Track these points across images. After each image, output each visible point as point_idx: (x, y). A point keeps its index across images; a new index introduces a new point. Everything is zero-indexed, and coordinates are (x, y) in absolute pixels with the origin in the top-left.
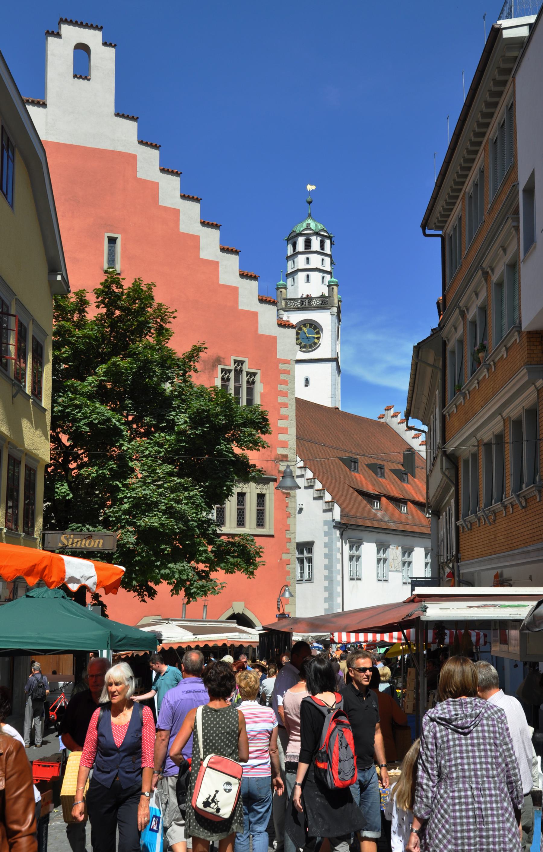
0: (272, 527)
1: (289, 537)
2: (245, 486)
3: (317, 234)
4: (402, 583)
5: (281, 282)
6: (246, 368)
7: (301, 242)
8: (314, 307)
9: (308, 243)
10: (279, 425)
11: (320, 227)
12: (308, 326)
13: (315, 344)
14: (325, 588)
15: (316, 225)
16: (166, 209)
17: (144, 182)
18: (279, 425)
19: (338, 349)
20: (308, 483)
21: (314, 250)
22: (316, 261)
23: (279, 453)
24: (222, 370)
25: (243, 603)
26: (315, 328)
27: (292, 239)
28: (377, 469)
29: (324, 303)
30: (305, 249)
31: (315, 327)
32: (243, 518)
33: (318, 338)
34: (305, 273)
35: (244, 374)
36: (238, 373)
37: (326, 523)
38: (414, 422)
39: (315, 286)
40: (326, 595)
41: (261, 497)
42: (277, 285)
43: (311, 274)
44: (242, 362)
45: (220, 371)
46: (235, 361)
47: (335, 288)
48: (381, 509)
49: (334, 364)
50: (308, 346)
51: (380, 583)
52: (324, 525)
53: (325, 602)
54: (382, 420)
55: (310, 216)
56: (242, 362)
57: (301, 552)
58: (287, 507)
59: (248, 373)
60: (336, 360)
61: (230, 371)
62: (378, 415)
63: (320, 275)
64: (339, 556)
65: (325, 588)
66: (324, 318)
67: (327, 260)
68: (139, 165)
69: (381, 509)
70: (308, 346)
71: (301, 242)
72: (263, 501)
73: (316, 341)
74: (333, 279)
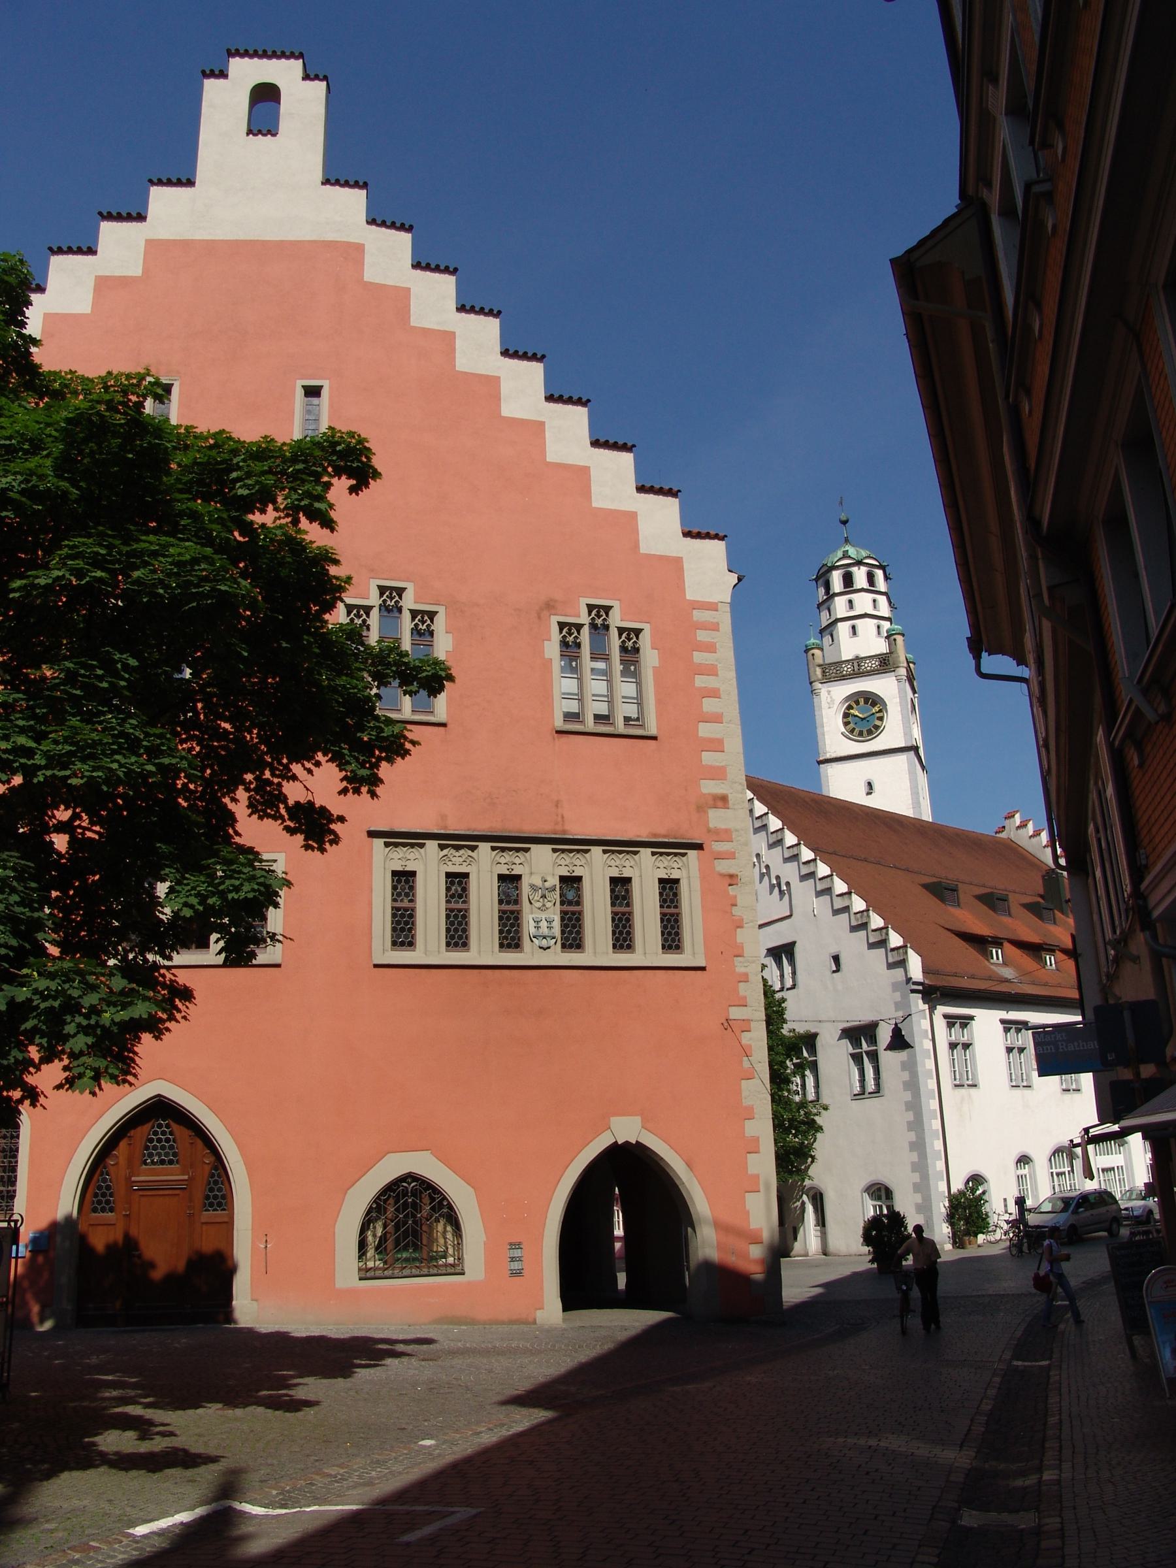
0: (700, 948)
1: (743, 970)
2: (627, 864)
3: (859, 563)
4: (1059, 1090)
5: (812, 641)
6: (616, 619)
7: (836, 579)
9: (848, 580)
10: (701, 734)
11: (864, 553)
12: (862, 701)
13: (877, 727)
14: (907, 1103)
16: (426, 332)
17: (378, 290)
18: (701, 734)
19: (916, 733)
20: (857, 920)
21: (859, 587)
22: (863, 603)
23: (705, 790)
24: (562, 626)
25: (638, 1119)
27: (823, 577)
28: (993, 901)
29: (885, 664)
31: (872, 699)
33: (881, 719)
35: (614, 633)
36: (599, 630)
37: (895, 987)
38: (995, 663)
39: (866, 642)
40: (910, 1116)
41: (669, 888)
44: (607, 609)
47: (899, 639)
48: (1005, 964)
50: (865, 733)
51: (1017, 1092)
52: (894, 991)
53: (909, 1130)
54: (1003, 835)
55: (847, 541)
57: (856, 1043)
59: (621, 630)
60: (915, 749)
62: (996, 829)
64: (928, 1045)
65: (907, 1103)
66: (887, 687)
67: (882, 600)
68: (368, 259)
69: (1005, 964)
70: (865, 733)
71: (836, 579)
72: (675, 895)
73: (878, 723)
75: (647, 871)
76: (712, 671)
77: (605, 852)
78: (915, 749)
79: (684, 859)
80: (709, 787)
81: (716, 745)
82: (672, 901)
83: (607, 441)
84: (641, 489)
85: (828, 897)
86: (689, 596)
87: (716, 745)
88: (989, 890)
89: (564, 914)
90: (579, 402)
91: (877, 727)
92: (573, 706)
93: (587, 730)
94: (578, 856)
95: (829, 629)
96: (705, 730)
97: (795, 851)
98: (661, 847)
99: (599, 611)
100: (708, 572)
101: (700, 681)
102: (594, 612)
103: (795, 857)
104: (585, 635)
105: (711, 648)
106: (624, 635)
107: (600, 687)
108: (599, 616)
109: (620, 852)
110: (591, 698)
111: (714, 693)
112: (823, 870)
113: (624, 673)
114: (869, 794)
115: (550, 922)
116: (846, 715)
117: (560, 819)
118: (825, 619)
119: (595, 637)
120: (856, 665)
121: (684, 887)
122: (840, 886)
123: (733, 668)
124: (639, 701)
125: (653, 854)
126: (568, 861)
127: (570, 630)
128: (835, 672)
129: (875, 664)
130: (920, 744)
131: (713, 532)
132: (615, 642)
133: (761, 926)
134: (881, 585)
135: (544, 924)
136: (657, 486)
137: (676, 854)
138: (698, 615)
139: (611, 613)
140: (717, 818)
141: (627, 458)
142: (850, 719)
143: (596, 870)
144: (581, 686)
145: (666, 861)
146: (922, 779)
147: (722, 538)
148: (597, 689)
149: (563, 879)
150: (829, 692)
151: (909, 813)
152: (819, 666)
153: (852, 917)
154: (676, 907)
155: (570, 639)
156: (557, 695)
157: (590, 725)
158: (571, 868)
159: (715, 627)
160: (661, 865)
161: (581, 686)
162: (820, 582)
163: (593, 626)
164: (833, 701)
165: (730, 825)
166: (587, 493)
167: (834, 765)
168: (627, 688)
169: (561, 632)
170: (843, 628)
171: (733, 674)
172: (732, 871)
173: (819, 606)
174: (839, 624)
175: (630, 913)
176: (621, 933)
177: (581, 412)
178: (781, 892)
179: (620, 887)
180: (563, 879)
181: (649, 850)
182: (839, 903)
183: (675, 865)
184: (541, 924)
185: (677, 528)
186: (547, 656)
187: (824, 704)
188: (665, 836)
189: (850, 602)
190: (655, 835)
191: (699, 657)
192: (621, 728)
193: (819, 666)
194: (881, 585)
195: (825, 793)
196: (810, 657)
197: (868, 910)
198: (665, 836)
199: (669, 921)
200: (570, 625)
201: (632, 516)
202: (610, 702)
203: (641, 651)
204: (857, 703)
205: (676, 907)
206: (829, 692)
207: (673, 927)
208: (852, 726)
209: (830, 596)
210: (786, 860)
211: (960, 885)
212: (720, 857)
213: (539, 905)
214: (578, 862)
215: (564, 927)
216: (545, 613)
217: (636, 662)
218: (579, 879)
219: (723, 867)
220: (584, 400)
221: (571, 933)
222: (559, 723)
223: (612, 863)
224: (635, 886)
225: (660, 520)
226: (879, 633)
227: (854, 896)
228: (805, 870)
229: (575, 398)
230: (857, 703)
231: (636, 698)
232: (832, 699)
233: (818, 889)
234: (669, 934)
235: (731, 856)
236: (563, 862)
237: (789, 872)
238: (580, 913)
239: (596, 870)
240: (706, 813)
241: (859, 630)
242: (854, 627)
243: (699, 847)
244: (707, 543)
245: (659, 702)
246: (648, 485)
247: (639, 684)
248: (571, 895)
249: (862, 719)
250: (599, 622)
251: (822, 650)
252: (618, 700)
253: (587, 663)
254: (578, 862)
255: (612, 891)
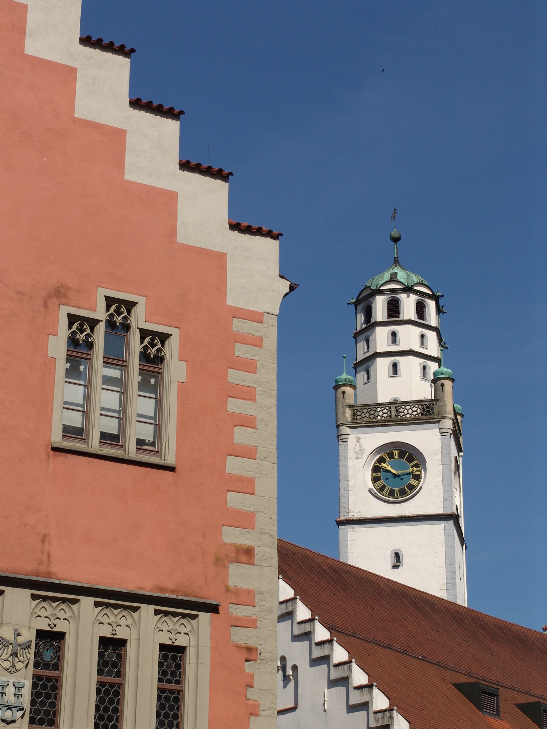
2: (123, 622)
3: (409, 290)
5: (344, 376)
6: (139, 319)
7: (380, 305)
8: (407, 420)
9: (394, 308)
10: (228, 470)
11: (415, 279)
12: (396, 454)
13: (412, 487)
15: (408, 276)
18: (228, 470)
19: (458, 499)
20: (377, 721)
22: (409, 337)
23: (227, 539)
24: (72, 319)
26: (410, 459)
29: (428, 412)
30: (389, 317)
31: (410, 455)
32: (116, 711)
33: (417, 478)
34: (390, 360)
35: (135, 335)
36: (118, 328)
39: (409, 384)
41: (172, 657)
42: (336, 381)
43: (401, 360)
44: (130, 305)
45: (64, 322)
46: (110, 301)
47: (448, 385)
49: (451, 523)
50: (397, 492)
55: (396, 262)
56: (130, 305)
58: (250, 686)
59: (144, 333)
60: (455, 518)
61: (93, 323)
63: (416, 362)
67: (432, 336)
70: (397, 492)
71: (380, 305)
72: (179, 667)
73: (413, 482)
74: (443, 369)
75: (145, 633)
76: (248, 394)
77: (97, 604)
78: (455, 518)
79: (194, 622)
80: (233, 536)
81: (246, 486)
82: (173, 674)
83: (150, 103)
84: (185, 166)
85: (343, 689)
86: (230, 301)
87: (246, 486)
88: (535, 700)
89: (37, 678)
90: (121, 51)
91: (412, 487)
92: (75, 420)
93: (90, 450)
94: (64, 606)
95: (366, 364)
96: (234, 466)
97: (307, 627)
98: (170, 605)
99: (120, 307)
100: (255, 275)
101: (234, 406)
102: (113, 308)
103: (307, 636)
104: (100, 334)
105: (250, 367)
106: (147, 340)
107: (109, 399)
108: (119, 313)
109: (116, 607)
110: (98, 412)
111: (249, 422)
112: (340, 654)
113: (144, 385)
114: (395, 567)
115: (18, 688)
116: (376, 469)
117: (45, 558)
118: (361, 352)
119: (113, 338)
120: (393, 410)
121: (190, 656)
122: (359, 677)
123: (275, 393)
124: (157, 421)
125: (157, 612)
126: (50, 611)
127: (81, 325)
128: (369, 416)
129: (416, 411)
130: (461, 513)
131: (265, 228)
132: (135, 346)
133: (280, 712)
134: (432, 319)
135: (10, 690)
136: (205, 165)
137: (184, 616)
138: (238, 325)
139: (134, 311)
140: (238, 576)
141: (172, 127)
142: (380, 474)
143: (84, 627)
144: (88, 396)
145: (171, 623)
146: (460, 555)
147: (276, 237)
148: (105, 400)
149: (40, 634)
150: (358, 440)
151: (442, 594)
152: (350, 406)
153: (372, 716)
154: (178, 682)
155: (81, 337)
156: (57, 405)
157: (94, 444)
158: (53, 621)
159: (257, 342)
160: (165, 627)
161: (88, 396)
162: (360, 307)
163: (111, 324)
164: (362, 450)
165: (253, 586)
166: (119, 162)
167: (357, 528)
168: (144, 405)
169: (70, 326)
170: (382, 365)
171: (273, 401)
172: (251, 643)
173: (356, 335)
174: (379, 360)
175: (121, 686)
176: (106, 709)
177: (123, 64)
178: (286, 678)
179: (112, 651)
180: (40, 634)
181: (152, 608)
182: (356, 698)
183: (182, 629)
184: (7, 690)
185: (223, 218)
186: (50, 354)
187: (351, 454)
188: (172, 592)
189: (394, 334)
190: (161, 589)
191: (235, 376)
192: (132, 452)
193: (350, 406)
194: (432, 319)
195: (341, 560)
196: (340, 395)
197: (391, 710)
198: (172, 592)
199: (167, 699)
200: (83, 320)
201: (171, 198)
202: (122, 419)
203: (166, 361)
204: (391, 456)
205: (178, 682)
206: (358, 440)
207: (171, 708)
208: (382, 482)
209: (371, 324)
210: (296, 638)
211: (501, 690)
212: (237, 623)
213: (7, 664)
214: (61, 615)
215: (36, 695)
216: (54, 300)
217: (158, 374)
218: (61, 636)
219: (241, 636)
220: (127, 48)
221: (43, 704)
222: (57, 438)
223: (105, 620)
224: (131, 650)
225: (204, 204)
226: (424, 375)
227: (376, 692)
228: (318, 653)
229: (117, 44)
230: (391, 456)
231: (154, 418)
232: (361, 448)
233: (332, 677)
234: (166, 716)
235: (251, 624)
236: (43, 613)
237: (298, 654)
238: (58, 680)
239: (84, 627)
240: (225, 567)
241: (402, 369)
242: (395, 365)
243: (213, 609)
244: (258, 240)
245: (181, 425)
246: (194, 162)
247: (159, 401)
248: (48, 655)
249: (395, 476)
250: (119, 319)
251: (354, 387)
252: (132, 418)
253: (101, 370)
254: (61, 615)
255: (101, 655)
